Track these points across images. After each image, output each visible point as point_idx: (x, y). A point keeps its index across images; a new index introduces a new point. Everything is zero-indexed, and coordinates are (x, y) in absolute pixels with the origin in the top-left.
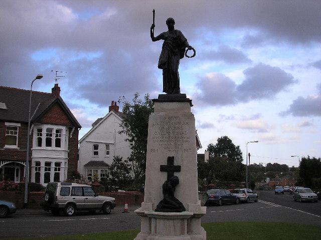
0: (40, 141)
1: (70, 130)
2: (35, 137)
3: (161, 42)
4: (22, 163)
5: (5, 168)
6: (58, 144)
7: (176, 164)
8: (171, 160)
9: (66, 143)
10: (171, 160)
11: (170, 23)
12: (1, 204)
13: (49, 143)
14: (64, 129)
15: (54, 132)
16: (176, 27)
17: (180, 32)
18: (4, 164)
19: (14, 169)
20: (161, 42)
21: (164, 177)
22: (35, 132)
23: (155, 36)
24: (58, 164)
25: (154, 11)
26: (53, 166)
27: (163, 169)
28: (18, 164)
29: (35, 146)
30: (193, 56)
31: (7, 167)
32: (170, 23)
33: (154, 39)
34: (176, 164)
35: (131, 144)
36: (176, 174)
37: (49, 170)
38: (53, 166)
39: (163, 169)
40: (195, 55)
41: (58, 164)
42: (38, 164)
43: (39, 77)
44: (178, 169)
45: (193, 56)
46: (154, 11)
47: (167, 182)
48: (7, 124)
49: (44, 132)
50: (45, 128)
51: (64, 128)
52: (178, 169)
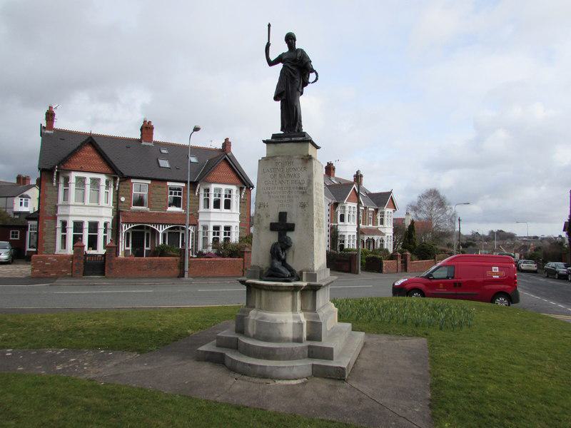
0: (207, 201)
1: (241, 189)
2: (202, 198)
3: (280, 66)
4: (152, 226)
5: (133, 232)
6: (228, 205)
7: (289, 221)
8: (283, 216)
9: (237, 205)
10: (283, 216)
11: (290, 39)
12: (569, 299)
13: (217, 205)
14: (234, 188)
15: (223, 193)
16: (298, 46)
17: (302, 50)
18: (166, 228)
19: (179, 233)
20: (280, 66)
21: (273, 238)
22: (202, 192)
23: (272, 58)
24: (227, 228)
25: (269, 25)
26: (222, 230)
27: (273, 227)
28: (148, 228)
29: (202, 209)
30: (315, 81)
31: (170, 231)
32: (290, 39)
33: (271, 63)
34: (289, 221)
35: (407, 214)
36: (289, 234)
37: (218, 234)
38: (222, 230)
39: (273, 227)
40: (317, 79)
41: (227, 228)
42: (205, 228)
43: (196, 129)
44: (291, 228)
45: (315, 81)
46: (269, 25)
47: (275, 244)
48: (169, 184)
49: (212, 192)
50: (213, 187)
51: (103, 178)
52: (291, 228)
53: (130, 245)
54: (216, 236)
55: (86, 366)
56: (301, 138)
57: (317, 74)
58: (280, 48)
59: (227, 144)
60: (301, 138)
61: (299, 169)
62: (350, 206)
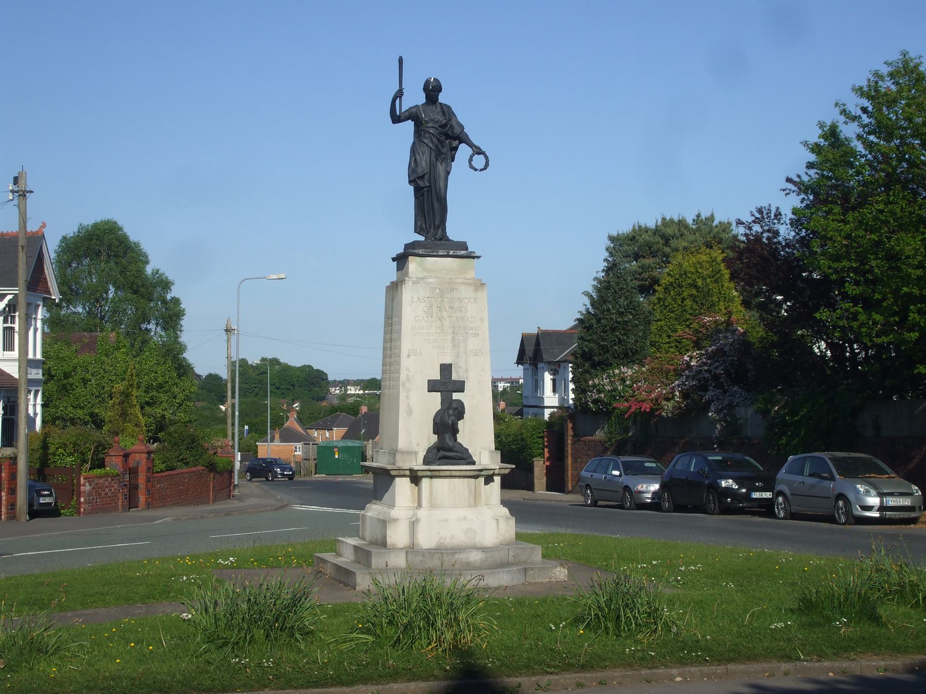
8: (446, 369)
21: (435, 401)
25: (401, 61)
27: (433, 386)
30: (485, 168)
32: (432, 90)
39: (433, 386)
44: (460, 387)
45: (481, 170)
46: (401, 61)
52: (460, 387)
53: (237, 397)
54: (9, 325)
55: (776, 570)
56: (463, 252)
57: (486, 158)
58: (414, 98)
59: (394, 260)
60: (463, 252)
61: (466, 301)
62: (118, 244)
